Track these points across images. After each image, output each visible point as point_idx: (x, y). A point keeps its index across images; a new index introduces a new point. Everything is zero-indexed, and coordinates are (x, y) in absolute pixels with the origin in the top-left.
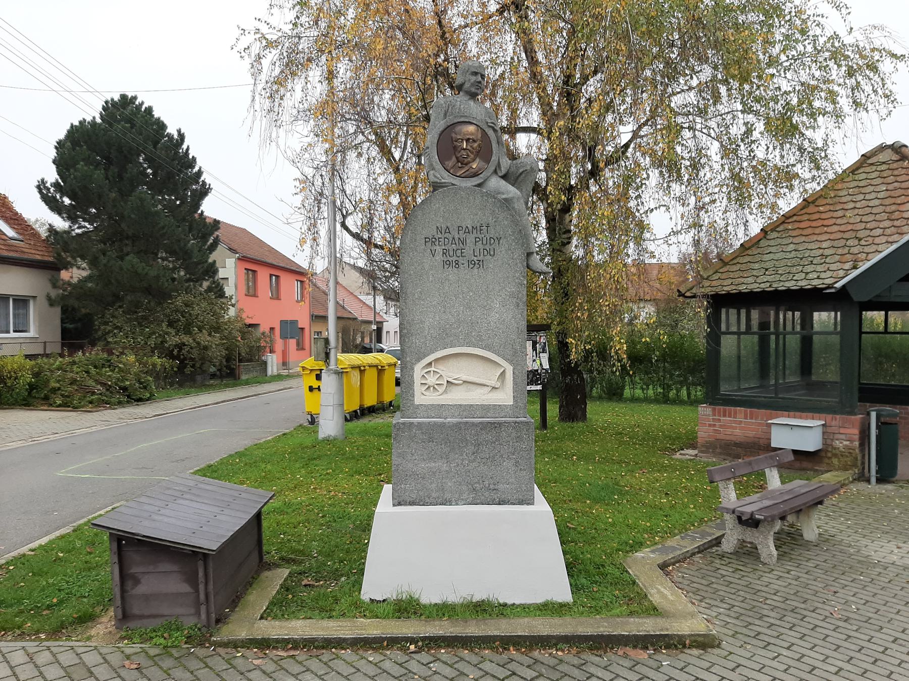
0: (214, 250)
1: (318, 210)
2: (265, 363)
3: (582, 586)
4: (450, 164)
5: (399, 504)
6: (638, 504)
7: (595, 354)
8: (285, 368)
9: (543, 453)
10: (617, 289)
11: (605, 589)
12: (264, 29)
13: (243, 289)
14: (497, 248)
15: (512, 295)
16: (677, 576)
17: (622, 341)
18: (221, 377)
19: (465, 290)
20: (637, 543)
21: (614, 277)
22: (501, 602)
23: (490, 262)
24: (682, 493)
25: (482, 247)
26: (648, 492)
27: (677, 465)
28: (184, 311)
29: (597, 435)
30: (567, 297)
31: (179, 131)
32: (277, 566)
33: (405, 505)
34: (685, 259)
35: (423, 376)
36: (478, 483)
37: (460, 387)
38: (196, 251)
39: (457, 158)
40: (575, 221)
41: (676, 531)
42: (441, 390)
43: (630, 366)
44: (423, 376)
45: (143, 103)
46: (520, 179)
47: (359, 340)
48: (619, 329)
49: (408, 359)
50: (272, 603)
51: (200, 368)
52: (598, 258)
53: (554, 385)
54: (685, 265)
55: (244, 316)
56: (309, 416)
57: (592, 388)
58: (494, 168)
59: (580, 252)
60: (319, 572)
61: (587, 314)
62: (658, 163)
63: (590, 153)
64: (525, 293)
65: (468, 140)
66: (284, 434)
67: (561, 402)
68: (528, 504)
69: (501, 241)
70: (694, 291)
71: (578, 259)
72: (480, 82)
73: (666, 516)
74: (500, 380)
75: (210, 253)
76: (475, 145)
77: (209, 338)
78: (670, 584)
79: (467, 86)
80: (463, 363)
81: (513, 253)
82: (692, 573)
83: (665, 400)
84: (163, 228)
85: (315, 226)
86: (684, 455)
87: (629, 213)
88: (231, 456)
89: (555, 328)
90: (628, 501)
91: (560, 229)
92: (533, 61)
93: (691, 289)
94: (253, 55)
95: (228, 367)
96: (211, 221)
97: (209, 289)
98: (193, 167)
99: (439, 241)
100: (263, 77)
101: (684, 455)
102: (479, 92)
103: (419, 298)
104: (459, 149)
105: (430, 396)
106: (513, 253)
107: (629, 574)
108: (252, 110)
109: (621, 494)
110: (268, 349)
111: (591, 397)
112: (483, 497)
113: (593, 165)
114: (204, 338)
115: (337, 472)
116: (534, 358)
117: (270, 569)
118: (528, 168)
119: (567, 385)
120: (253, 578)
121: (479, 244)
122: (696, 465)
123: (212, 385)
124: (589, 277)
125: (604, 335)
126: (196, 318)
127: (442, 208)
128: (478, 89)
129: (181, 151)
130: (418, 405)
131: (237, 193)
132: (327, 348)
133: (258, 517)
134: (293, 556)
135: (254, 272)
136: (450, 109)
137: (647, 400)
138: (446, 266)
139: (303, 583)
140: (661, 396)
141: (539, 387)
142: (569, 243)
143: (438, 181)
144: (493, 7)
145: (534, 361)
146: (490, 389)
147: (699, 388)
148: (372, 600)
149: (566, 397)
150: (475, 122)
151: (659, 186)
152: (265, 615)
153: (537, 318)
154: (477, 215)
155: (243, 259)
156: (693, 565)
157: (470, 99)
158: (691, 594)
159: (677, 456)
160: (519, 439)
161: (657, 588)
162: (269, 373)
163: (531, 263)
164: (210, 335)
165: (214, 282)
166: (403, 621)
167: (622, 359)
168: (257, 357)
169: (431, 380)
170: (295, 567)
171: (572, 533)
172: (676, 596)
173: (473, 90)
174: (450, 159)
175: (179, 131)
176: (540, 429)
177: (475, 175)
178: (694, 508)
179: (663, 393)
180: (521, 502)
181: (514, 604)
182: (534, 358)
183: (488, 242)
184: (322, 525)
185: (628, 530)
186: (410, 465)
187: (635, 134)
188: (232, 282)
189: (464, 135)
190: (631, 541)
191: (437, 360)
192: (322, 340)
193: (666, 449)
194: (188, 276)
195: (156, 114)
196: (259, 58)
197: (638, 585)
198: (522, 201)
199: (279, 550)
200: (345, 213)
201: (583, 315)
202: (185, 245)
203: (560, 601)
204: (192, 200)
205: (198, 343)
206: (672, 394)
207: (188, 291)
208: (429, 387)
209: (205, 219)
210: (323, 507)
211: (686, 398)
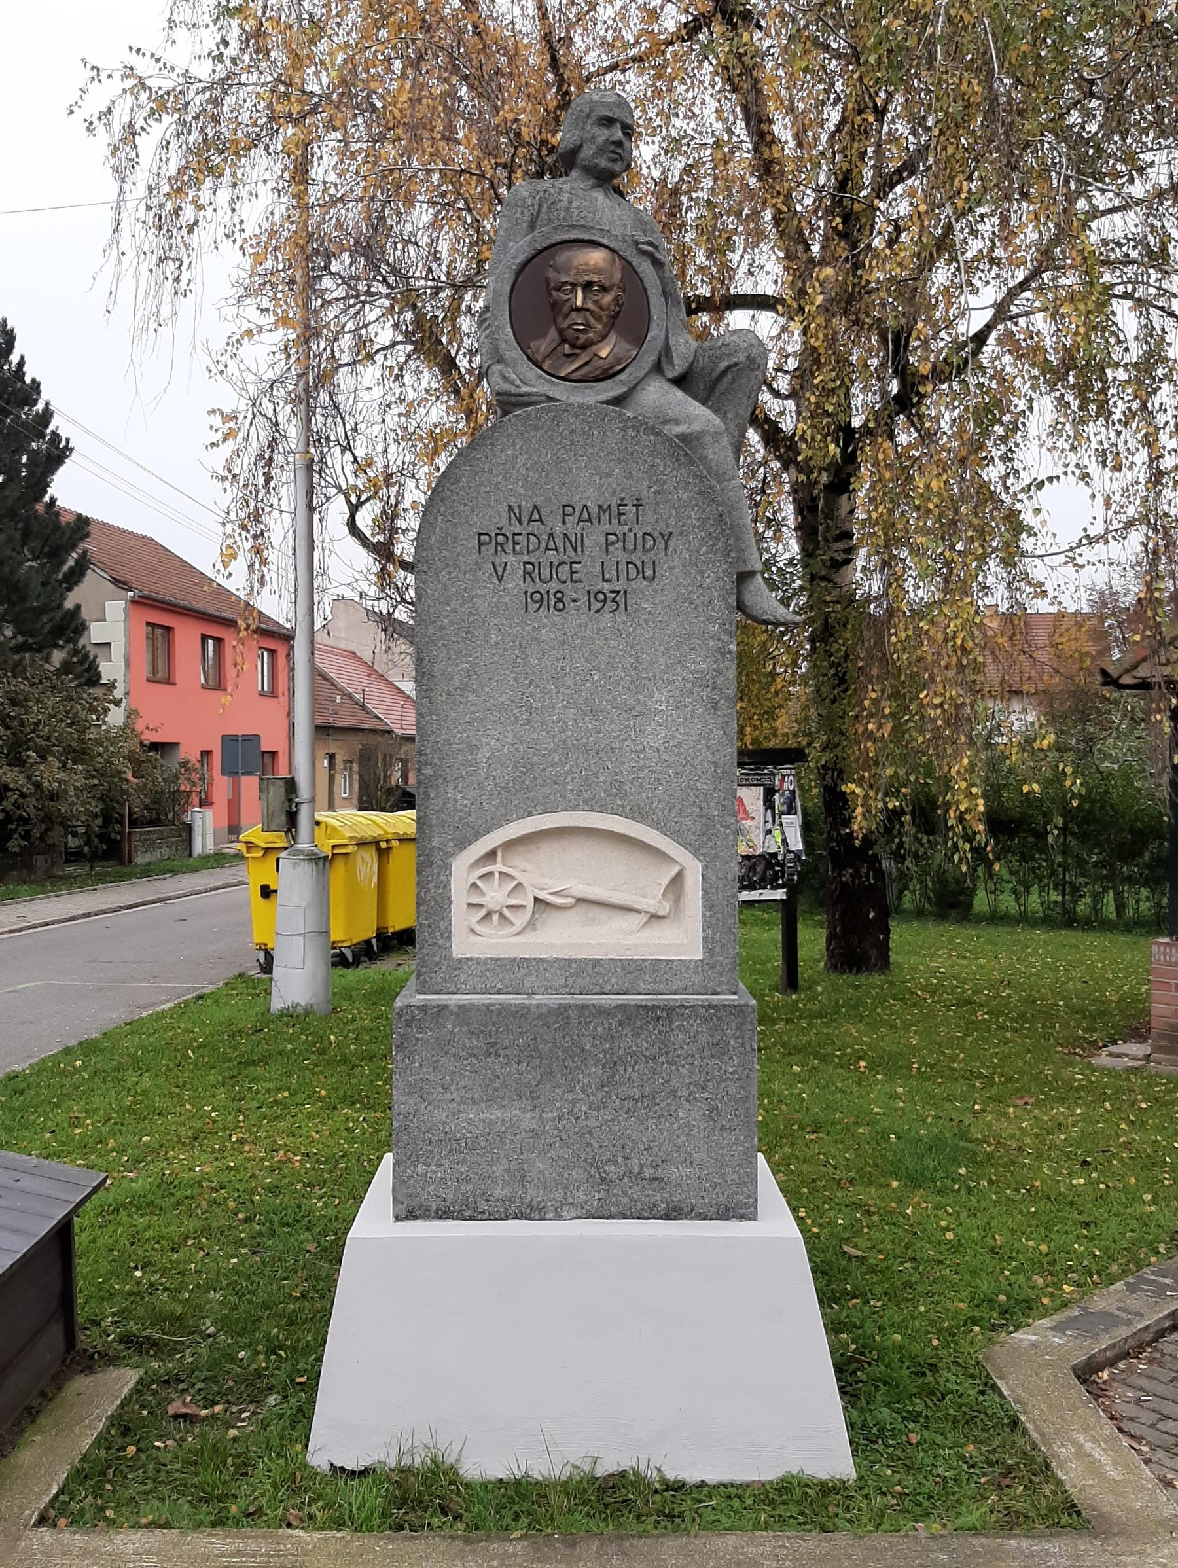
0: (76, 583)
1: (267, 482)
2: (189, 828)
3: (882, 1430)
4: (543, 346)
5: (411, 1215)
6: (1017, 1190)
7: (908, 818)
8: (233, 837)
9: (791, 1051)
10: (961, 668)
11: (939, 1439)
12: (144, 67)
13: (144, 670)
15: (699, 680)
16: (1122, 1398)
17: (974, 790)
18: (95, 858)
20: (1018, 1303)
21: (954, 637)
22: (671, 1476)
23: (646, 597)
24: (1121, 1160)
25: (623, 557)
26: (1039, 1157)
27: (1106, 1086)
28: (8, 715)
29: (914, 1005)
30: (843, 687)
32: (111, 1360)
33: (426, 1216)
34: (1105, 604)
35: (474, 884)
36: (613, 1161)
37: (568, 914)
38: (36, 586)
39: (560, 332)
40: (860, 514)
41: (1114, 1268)
42: (520, 920)
43: (993, 850)
44: (474, 884)
46: (722, 386)
47: (396, 777)
48: (966, 761)
49: (435, 842)
50: (79, 1475)
51: (41, 839)
52: (918, 592)
53: (815, 883)
54: (1102, 618)
55: (139, 726)
56: (262, 954)
57: (901, 892)
58: (654, 358)
59: (875, 585)
60: (214, 1379)
61: (889, 726)
62: (1054, 375)
63: (898, 342)
65: (587, 286)
66: (200, 997)
67: (831, 926)
68: (741, 1217)
69: (672, 543)
70: (1143, 672)
71: (868, 600)
72: (619, 144)
73: (1087, 1225)
74: (671, 896)
75: (69, 589)
76: (607, 299)
77: (61, 775)
78: (1109, 1429)
79: (587, 152)
80: (576, 853)
81: (701, 572)
82: (1159, 1389)
83: (1068, 920)
85: (256, 517)
86: (1119, 1056)
87: (985, 494)
88: (67, 1051)
89: (816, 756)
90: (991, 1182)
91: (828, 528)
92: (762, 136)
93: (1135, 667)
94: (117, 127)
95: (103, 837)
96: (71, 519)
97: (66, 667)
98: (35, 402)
100: (141, 177)
101: (1119, 1056)
102: (617, 167)
103: (464, 688)
104: (566, 309)
105: (491, 936)
106: (701, 572)
107: (1001, 1395)
108: (114, 252)
109: (977, 1162)
110: (195, 800)
111: (899, 911)
112: (625, 1200)
113: (903, 384)
114: (50, 774)
115: (300, 1097)
116: (769, 825)
117: (89, 1369)
118: (742, 358)
119: (844, 886)
120: (43, 1394)
121: (617, 552)
122: (1150, 1085)
123: (69, 876)
124: (894, 639)
125: (929, 773)
126: (33, 731)
127: (520, 461)
128: (614, 161)
129: (6, 367)
130: (460, 961)
131: (108, 445)
132: (290, 801)
133: (63, 1233)
134: (155, 1334)
135: (168, 629)
136: (544, 210)
137: (1025, 919)
139: (171, 1410)
140: (1058, 909)
141: (780, 894)
142: (848, 561)
143: (513, 390)
144: (672, 20)
145: (769, 832)
146: (643, 918)
147: (1144, 892)
148: (338, 1471)
149: (842, 917)
150: (605, 242)
151: (1056, 430)
152: (52, 1513)
153: (775, 735)
154: (609, 475)
155: (143, 602)
156: (1160, 1364)
157: (593, 187)
158: (1160, 1454)
159: (1103, 1059)
160: (719, 1048)
161: (1074, 1443)
162: (197, 849)
163: (749, 599)
164: (64, 767)
165: (76, 652)
166: (407, 1538)
167: (975, 833)
168: (170, 816)
169: (495, 895)
170: (155, 1364)
171: (856, 1271)
172: (1126, 1466)
173: (603, 163)
174: (543, 334)
176: (784, 993)
177: (607, 375)
178: (1154, 1201)
179: (1063, 903)
180: (723, 1214)
181: (703, 1484)
182: (769, 825)
183: (639, 547)
184: (240, 1243)
185: (991, 1262)
186: (440, 1115)
187: (1001, 311)
188: (118, 651)
189: (578, 273)
190: (1002, 1298)
191: (510, 845)
192: (281, 783)
193: (1076, 1041)
194: (20, 639)
196: (131, 133)
197: (1025, 1432)
198: (725, 441)
199: (123, 1315)
200: (353, 499)
201: (880, 727)
202: (12, 572)
203: (824, 1476)
204: (31, 473)
205: (38, 786)
206: (1083, 906)
207: (17, 670)
208: (488, 915)
209: (57, 514)
210: (253, 1192)
211: (1113, 916)
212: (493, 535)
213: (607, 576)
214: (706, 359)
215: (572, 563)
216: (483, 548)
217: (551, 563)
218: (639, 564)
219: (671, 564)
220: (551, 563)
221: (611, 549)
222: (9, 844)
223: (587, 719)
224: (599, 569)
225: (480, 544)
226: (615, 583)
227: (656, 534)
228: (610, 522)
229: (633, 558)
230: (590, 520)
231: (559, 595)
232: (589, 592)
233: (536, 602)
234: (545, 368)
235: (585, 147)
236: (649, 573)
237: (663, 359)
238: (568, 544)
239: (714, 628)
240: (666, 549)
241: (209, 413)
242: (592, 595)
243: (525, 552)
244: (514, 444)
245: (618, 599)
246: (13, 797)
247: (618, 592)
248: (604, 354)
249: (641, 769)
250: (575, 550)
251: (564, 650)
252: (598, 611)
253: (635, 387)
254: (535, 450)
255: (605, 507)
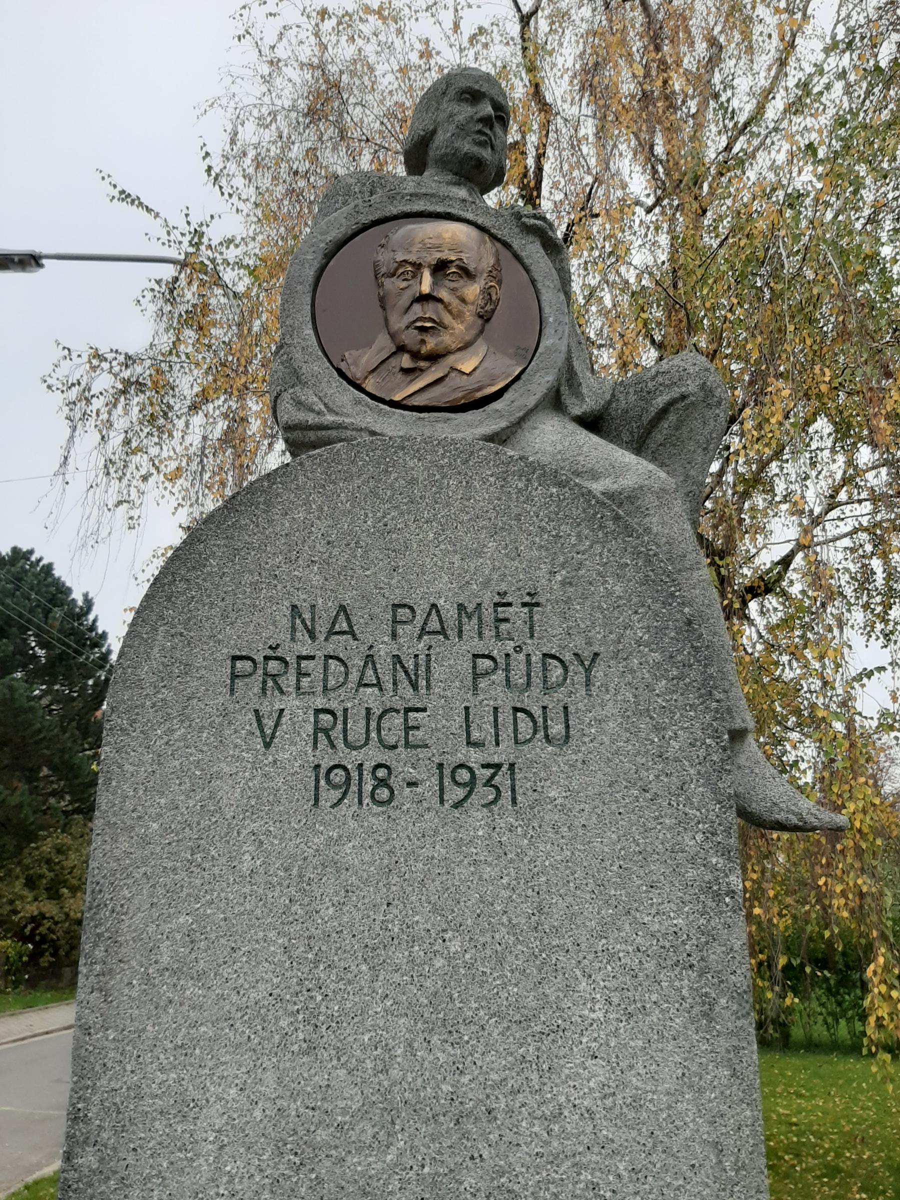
14: (579, 701)
19: (422, 921)
25: (506, 700)
31: (86, 596)
45: (39, 560)
64: (739, 938)
69: (598, 673)
81: (658, 728)
84: (40, 731)
98: (103, 646)
99: (301, 674)
138: (329, 796)
143: (312, 419)
150: (469, 216)
154: (479, 554)
175: (86, 596)
183: (536, 680)
195: (57, 573)
202: (71, 758)
212: (259, 658)
213: (476, 735)
214: (632, 398)
215: (408, 710)
216: (239, 683)
217: (368, 710)
218: (537, 712)
219: (597, 712)
220: (368, 710)
221: (483, 684)
222: (41, 960)
223: (435, 1039)
224: (460, 720)
225: (234, 676)
226: (492, 749)
227: (567, 657)
228: (480, 634)
229: (526, 702)
230: (443, 632)
231: (381, 773)
232: (440, 766)
233: (336, 787)
234: (369, 388)
235: (440, 132)
236: (557, 729)
237: (564, 389)
238: (401, 675)
239: (691, 842)
240: (588, 683)
241: (125, 610)
242: (447, 772)
243: (320, 689)
244: (307, 503)
245: (497, 780)
246: (47, 924)
247: (498, 766)
248: (467, 367)
249: (555, 1160)
250: (415, 686)
251: (388, 885)
252: (457, 805)
253: (520, 423)
254: (345, 513)
255: (471, 608)
